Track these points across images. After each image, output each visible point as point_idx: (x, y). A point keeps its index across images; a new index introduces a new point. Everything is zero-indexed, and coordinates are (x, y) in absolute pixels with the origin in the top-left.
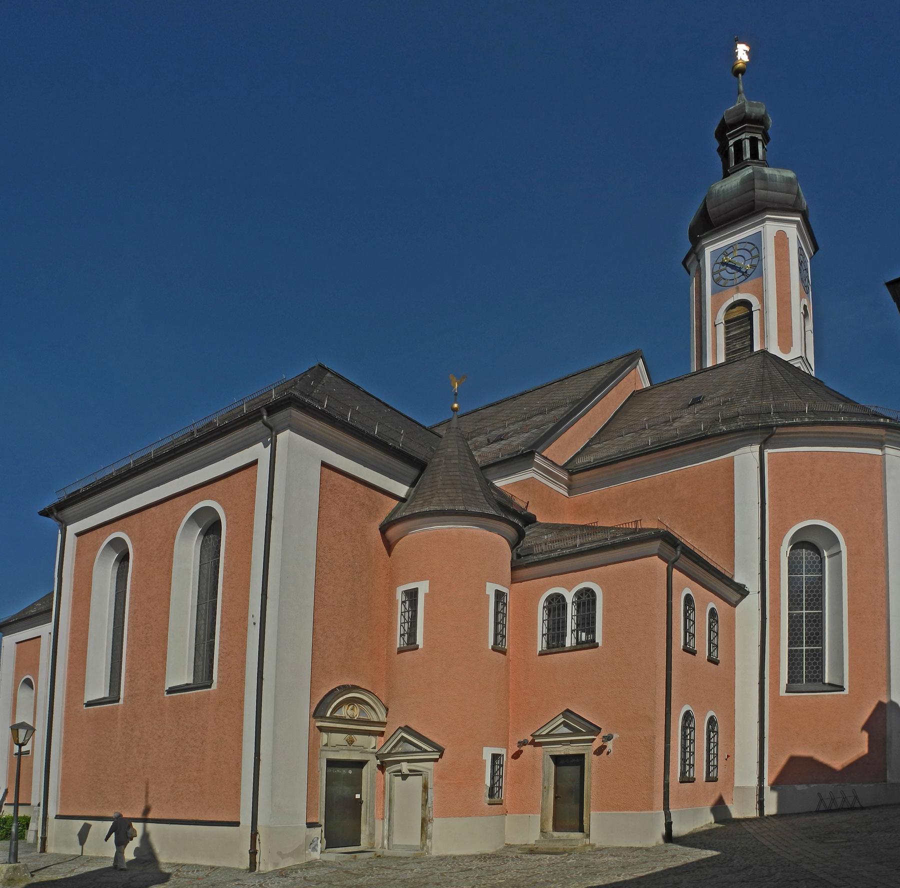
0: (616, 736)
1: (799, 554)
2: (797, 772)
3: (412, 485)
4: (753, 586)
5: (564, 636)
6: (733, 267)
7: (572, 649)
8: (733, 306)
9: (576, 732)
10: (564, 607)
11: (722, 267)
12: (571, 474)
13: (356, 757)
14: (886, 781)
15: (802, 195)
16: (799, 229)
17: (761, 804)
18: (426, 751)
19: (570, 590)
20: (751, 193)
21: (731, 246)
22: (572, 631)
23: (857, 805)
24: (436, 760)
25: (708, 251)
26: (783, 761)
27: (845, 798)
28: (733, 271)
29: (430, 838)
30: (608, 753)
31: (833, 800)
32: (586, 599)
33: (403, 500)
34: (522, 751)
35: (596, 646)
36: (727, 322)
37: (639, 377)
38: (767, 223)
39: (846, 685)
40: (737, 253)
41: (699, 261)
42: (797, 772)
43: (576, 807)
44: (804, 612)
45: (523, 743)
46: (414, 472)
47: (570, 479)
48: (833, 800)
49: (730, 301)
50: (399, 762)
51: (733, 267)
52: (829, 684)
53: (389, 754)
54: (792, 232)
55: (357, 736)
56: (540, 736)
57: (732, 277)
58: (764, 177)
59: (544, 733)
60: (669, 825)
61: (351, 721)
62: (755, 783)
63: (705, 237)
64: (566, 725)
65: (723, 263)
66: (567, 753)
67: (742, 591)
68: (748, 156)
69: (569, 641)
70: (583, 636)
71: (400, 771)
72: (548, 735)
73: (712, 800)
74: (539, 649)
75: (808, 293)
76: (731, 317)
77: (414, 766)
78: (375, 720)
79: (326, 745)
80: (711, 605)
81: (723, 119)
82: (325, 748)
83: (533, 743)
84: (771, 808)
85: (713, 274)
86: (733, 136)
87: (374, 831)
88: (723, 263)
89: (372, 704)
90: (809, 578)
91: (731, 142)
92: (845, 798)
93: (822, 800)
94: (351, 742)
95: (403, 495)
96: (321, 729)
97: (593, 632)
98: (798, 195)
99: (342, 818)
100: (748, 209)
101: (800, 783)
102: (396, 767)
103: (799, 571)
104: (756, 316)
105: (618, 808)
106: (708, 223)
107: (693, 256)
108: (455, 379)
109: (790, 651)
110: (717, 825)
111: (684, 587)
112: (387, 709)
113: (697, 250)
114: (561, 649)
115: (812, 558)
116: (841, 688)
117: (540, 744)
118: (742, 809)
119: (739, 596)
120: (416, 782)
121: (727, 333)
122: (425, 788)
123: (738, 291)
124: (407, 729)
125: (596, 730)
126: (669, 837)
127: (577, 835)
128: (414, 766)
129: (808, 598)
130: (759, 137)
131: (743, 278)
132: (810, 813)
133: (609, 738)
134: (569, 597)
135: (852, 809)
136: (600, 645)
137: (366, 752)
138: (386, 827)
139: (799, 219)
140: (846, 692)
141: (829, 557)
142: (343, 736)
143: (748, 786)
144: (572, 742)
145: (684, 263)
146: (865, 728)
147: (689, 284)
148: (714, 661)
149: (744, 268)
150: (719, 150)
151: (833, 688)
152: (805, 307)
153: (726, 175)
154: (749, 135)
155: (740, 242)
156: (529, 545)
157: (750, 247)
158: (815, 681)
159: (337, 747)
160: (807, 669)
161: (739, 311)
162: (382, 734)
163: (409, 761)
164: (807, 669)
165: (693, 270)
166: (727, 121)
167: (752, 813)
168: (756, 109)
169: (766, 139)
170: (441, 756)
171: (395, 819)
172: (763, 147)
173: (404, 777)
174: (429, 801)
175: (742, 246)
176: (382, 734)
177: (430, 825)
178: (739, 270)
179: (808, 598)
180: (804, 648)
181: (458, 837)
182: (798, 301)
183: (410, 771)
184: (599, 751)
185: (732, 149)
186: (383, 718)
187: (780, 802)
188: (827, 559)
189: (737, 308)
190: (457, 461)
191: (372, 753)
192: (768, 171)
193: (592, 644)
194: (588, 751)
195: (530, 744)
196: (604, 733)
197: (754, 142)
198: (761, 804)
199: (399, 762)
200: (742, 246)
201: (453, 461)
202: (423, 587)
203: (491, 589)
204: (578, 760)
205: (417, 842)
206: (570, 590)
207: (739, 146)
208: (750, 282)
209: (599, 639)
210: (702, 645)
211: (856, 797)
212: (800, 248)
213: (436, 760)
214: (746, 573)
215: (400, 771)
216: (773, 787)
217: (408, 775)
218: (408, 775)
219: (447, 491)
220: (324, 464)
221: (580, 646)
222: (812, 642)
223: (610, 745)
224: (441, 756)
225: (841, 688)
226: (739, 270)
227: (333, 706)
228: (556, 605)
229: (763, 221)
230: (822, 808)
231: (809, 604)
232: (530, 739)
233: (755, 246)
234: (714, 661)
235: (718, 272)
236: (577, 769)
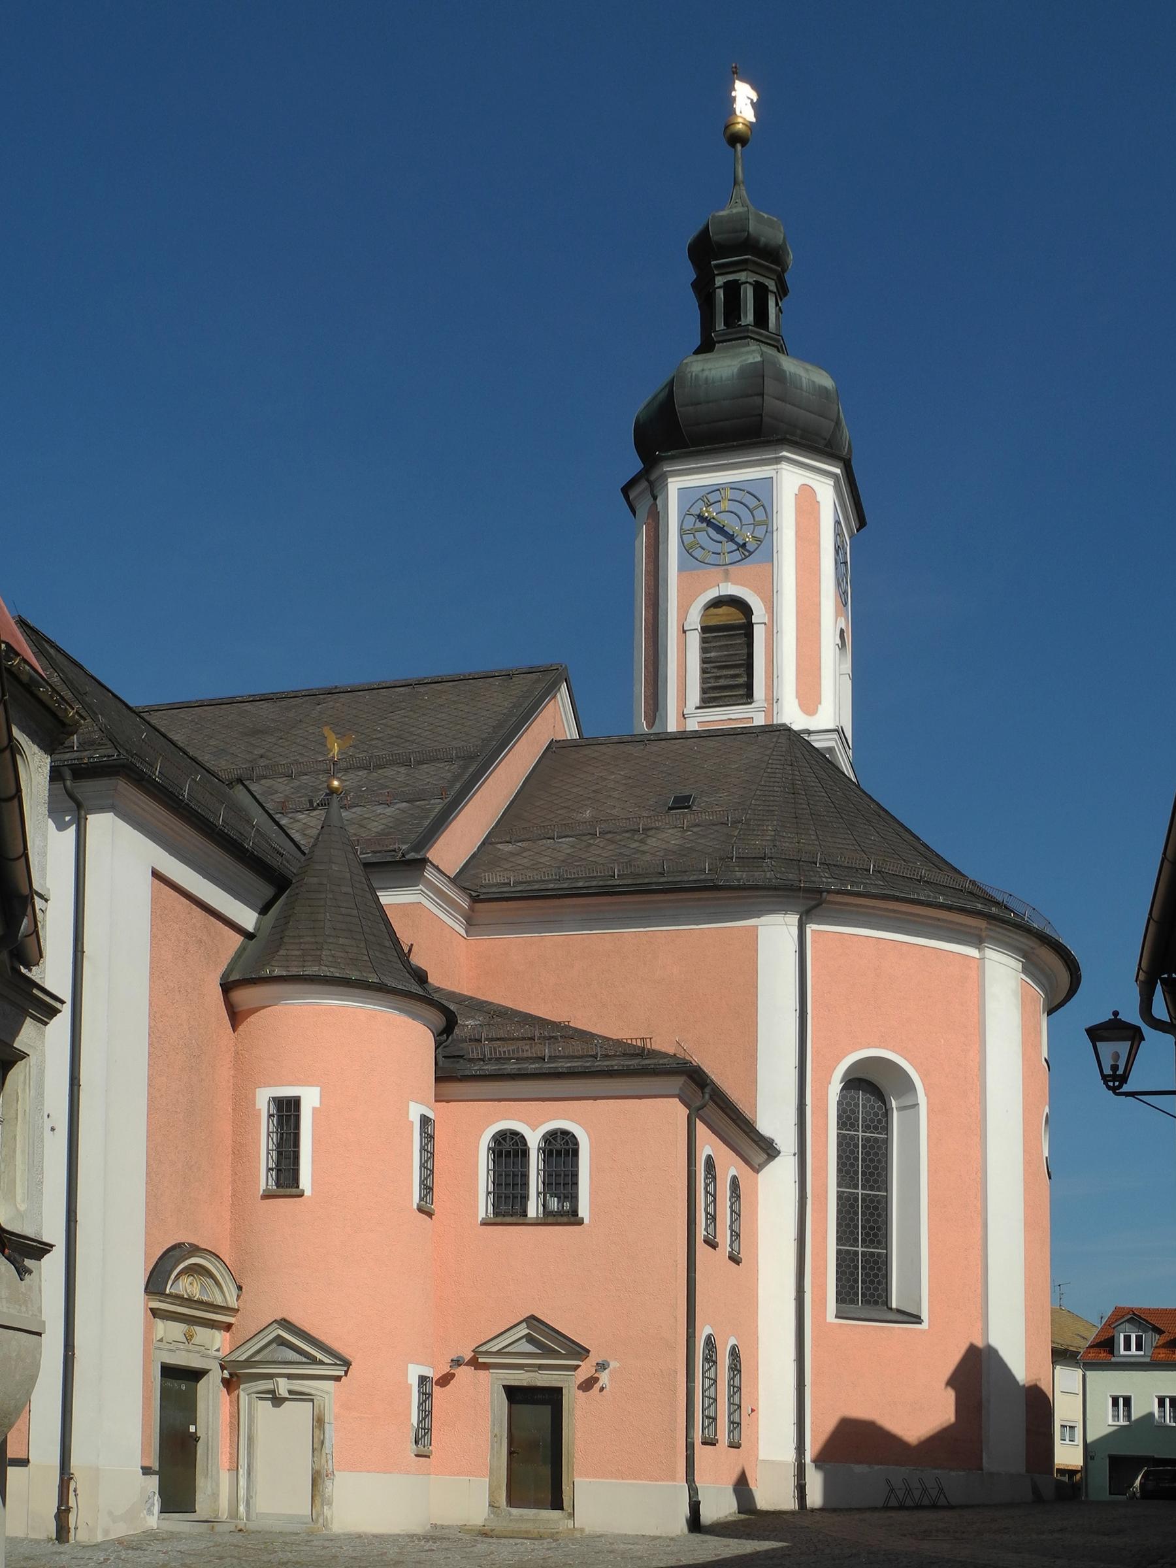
0: (613, 1364)
1: (853, 1098)
2: (854, 1445)
3: (263, 911)
4: (786, 1141)
5: (525, 1198)
6: (720, 530)
7: (536, 1223)
8: (718, 603)
9: (549, 1352)
10: (525, 1153)
11: (699, 525)
12: (475, 900)
13: (195, 1363)
14: (982, 1469)
15: (844, 423)
16: (837, 487)
17: (801, 1489)
18: (321, 1363)
19: (534, 1128)
20: (758, 400)
21: (717, 489)
22: (538, 1193)
23: (942, 1501)
24: (338, 1379)
25: (675, 486)
26: (830, 1425)
27: (925, 1490)
28: (719, 537)
29: (330, 1504)
30: (602, 1389)
31: (909, 1491)
32: (561, 1148)
33: (249, 936)
34: (453, 1375)
35: (580, 1222)
36: (705, 629)
37: (558, 720)
38: (784, 466)
39: (925, 1316)
40: (726, 505)
41: (655, 498)
42: (854, 1445)
43: (546, 1471)
44: (860, 1191)
45: (457, 1362)
46: (268, 891)
47: (471, 909)
48: (909, 1491)
49: (712, 594)
50: (270, 1376)
51: (720, 530)
52: (899, 1311)
53: (248, 1363)
54: (826, 492)
55: (198, 1329)
56: (487, 1353)
57: (717, 547)
58: (780, 376)
59: (495, 1349)
60: (695, 1507)
61: (189, 1301)
62: (790, 1456)
63: (673, 458)
64: (530, 1339)
65: (701, 518)
66: (533, 1384)
67: (769, 1150)
68: (750, 318)
69: (533, 1209)
70: (554, 1204)
71: (273, 1392)
72: (499, 1353)
73: (734, 1476)
74: (482, 1214)
75: (845, 604)
76: (713, 622)
77: (299, 1385)
78: (219, 1301)
79: (161, 1340)
80: (733, 1172)
81: (706, 230)
82: (160, 1345)
83: (474, 1363)
84: (815, 1498)
85: (682, 532)
86: (725, 269)
87: (216, 1487)
88: (701, 518)
89: (219, 1277)
90: (868, 1139)
91: (719, 281)
92: (925, 1490)
93: (892, 1490)
94: (189, 1337)
95: (250, 927)
96: (155, 1313)
97: (574, 1198)
98: (838, 423)
99: (176, 1460)
100: (749, 427)
101: (860, 1463)
102: (267, 1385)
103: (852, 1125)
104: (759, 633)
105: (621, 1475)
106: (672, 432)
107: (644, 484)
108: (333, 736)
109: (839, 1252)
110: (743, 1516)
111: (708, 1145)
112: (240, 1288)
113: (653, 477)
114: (521, 1220)
115: (872, 1107)
116: (917, 1319)
117: (486, 1367)
118: (774, 1494)
119: (765, 1156)
120: (299, 1412)
121: (704, 650)
122: (319, 1422)
123: (727, 578)
124: (285, 1323)
125: (581, 1352)
126: (695, 1523)
127: (556, 1514)
128: (299, 1385)
129: (866, 1166)
130: (771, 285)
131: (737, 556)
132: (874, 1509)
133: (602, 1366)
134: (534, 1140)
135: (934, 1507)
136: (586, 1221)
137: (208, 1357)
138: (243, 1482)
139: (838, 471)
140: (925, 1326)
141: (900, 1109)
142: (182, 1327)
143: (775, 1456)
144: (541, 1367)
145: (626, 490)
146: (951, 1383)
147: (635, 535)
148: (735, 1259)
149: (737, 536)
150: (694, 285)
151: (905, 1318)
152: (842, 631)
153: (706, 346)
154: (753, 278)
155: (734, 487)
156: (475, 1050)
157: (752, 503)
158: (876, 1303)
159: (179, 1344)
160: (865, 1282)
161: (727, 615)
162: (228, 1327)
163: (290, 1377)
164: (865, 1282)
165: (643, 509)
166: (715, 237)
167: (788, 1503)
168: (768, 228)
169: (783, 291)
170: (346, 1373)
171: (261, 1466)
172: (777, 304)
173: (277, 1401)
174: (327, 1443)
175: (738, 495)
176: (228, 1327)
177: (328, 1483)
178: (731, 538)
179: (866, 1166)
180: (860, 1249)
181: (375, 1502)
182: (831, 621)
183: (290, 1392)
184: (587, 1385)
185: (720, 294)
186: (233, 1304)
187: (829, 1488)
188: (895, 1113)
189: (724, 610)
190: (350, 890)
191: (215, 1358)
192: (788, 364)
193: (571, 1217)
194: (569, 1383)
195: (468, 1364)
196: (593, 1359)
197: (761, 293)
198: (801, 1489)
199: (270, 1376)
200: (738, 495)
201: (344, 889)
202: (310, 1099)
203: (415, 1111)
204: (552, 1398)
205: (302, 1507)
206: (534, 1128)
207: (733, 289)
208: (747, 568)
209: (584, 1211)
210: (724, 1237)
211: (941, 1490)
212: (837, 523)
213: (338, 1379)
214: (774, 1118)
215: (273, 1392)
216: (819, 1461)
217: (286, 1399)
218: (286, 1399)
219: (341, 941)
220: (156, 874)
221: (550, 1218)
222: (872, 1241)
223: (604, 1378)
224: (346, 1373)
225: (917, 1319)
226: (731, 538)
227: (173, 1276)
228: (508, 1149)
229: (778, 460)
230: (893, 1502)
231: (867, 1181)
232: (468, 1356)
233: (759, 503)
234: (735, 1259)
235: (693, 531)
236: (546, 1410)
